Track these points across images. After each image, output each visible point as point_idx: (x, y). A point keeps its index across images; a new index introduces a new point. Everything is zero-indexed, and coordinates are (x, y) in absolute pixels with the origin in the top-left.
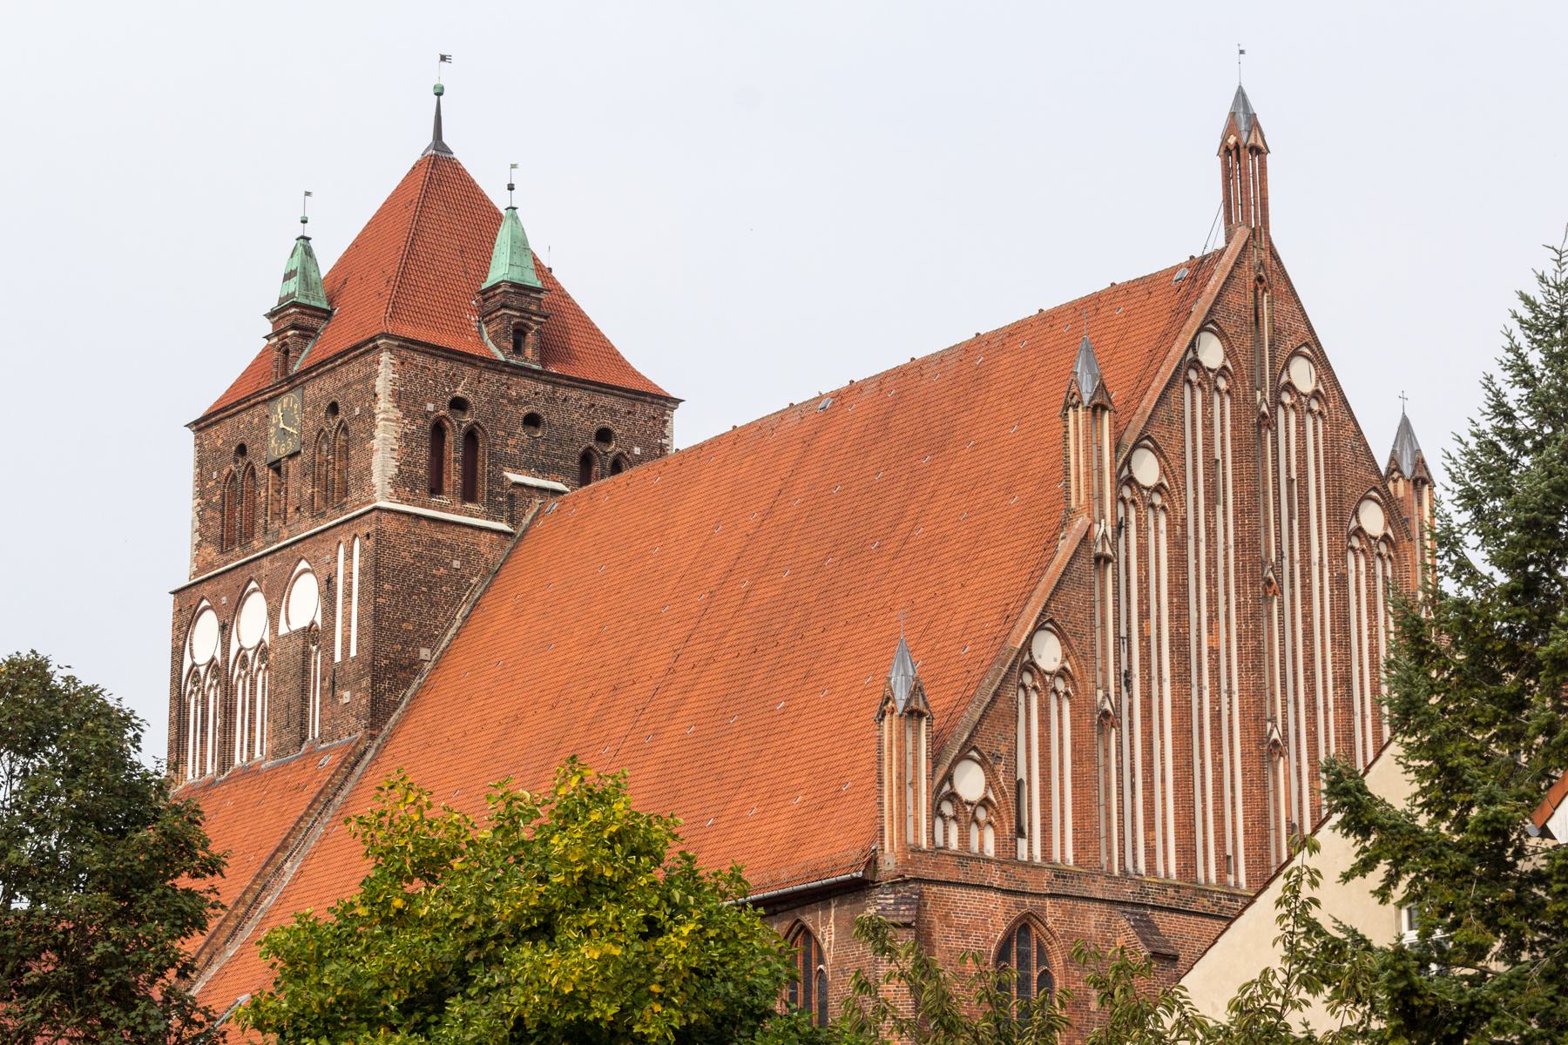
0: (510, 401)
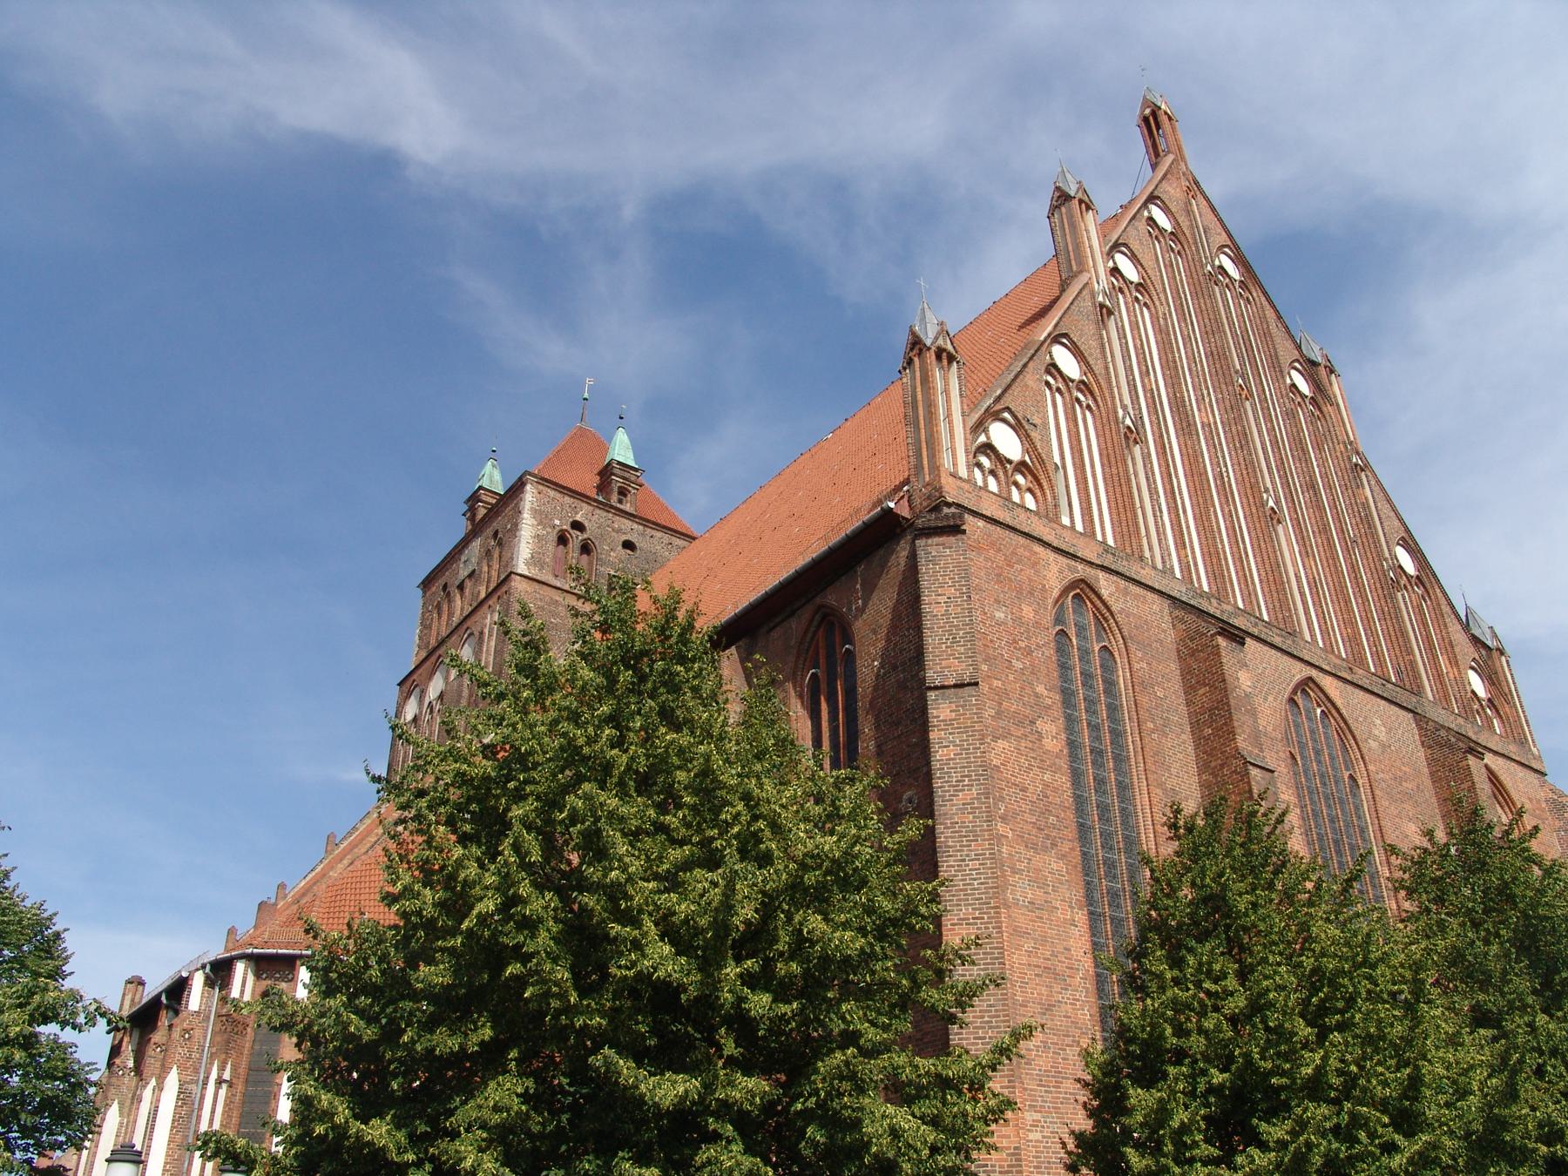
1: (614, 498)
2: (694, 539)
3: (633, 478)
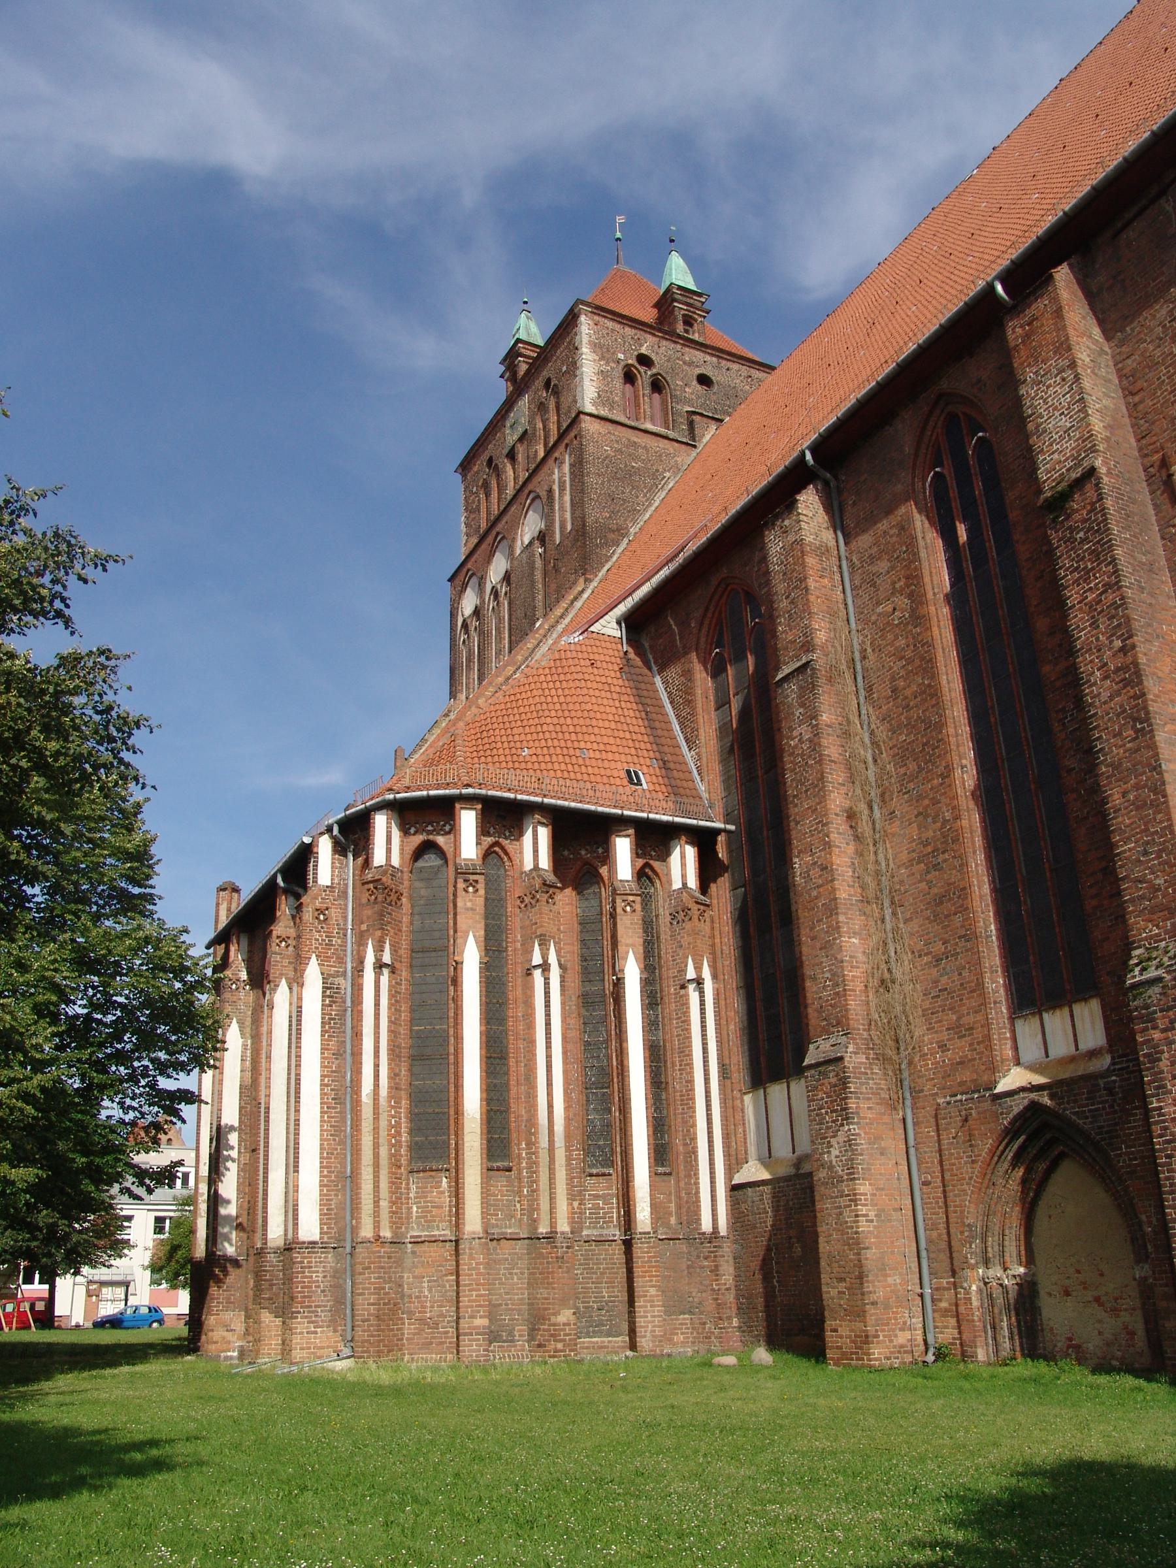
0: (685, 363)
1: (680, 328)
2: (773, 368)
3: (699, 305)
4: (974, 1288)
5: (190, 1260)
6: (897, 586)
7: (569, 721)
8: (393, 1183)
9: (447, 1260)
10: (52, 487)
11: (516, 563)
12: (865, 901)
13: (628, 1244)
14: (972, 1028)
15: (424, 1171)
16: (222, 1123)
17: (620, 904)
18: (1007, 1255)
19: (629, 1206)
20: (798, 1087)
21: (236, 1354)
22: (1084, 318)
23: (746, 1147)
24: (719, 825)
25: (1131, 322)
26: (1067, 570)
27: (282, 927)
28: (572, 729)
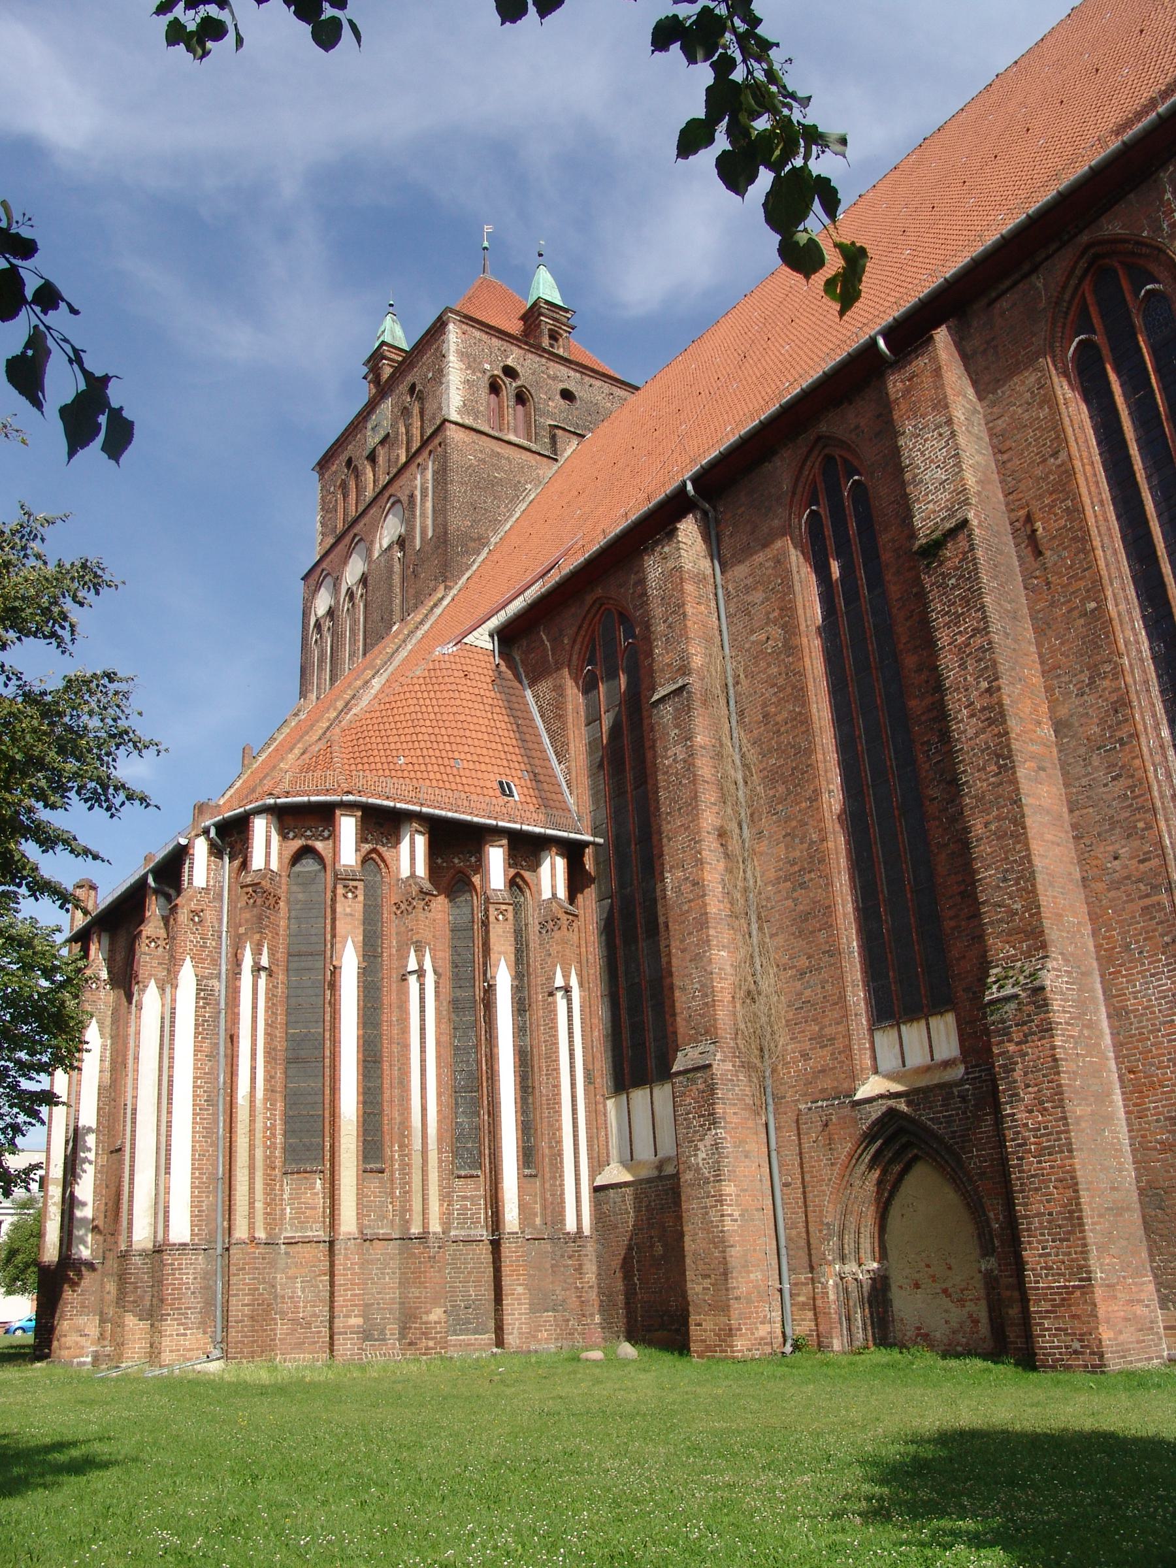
1: (546, 342)
3: (565, 320)
4: (831, 1282)
5: (37, 1263)
6: (771, 616)
7: (443, 731)
8: (267, 1184)
9: (320, 1261)
10: (61, 515)
11: (373, 566)
12: (734, 915)
13: (496, 1245)
14: (834, 1039)
15: (298, 1173)
16: (80, 1125)
17: (492, 912)
18: (862, 1251)
19: (497, 1207)
20: (663, 1093)
21: (89, 1359)
22: (960, 378)
23: (608, 1149)
24: (588, 838)
25: (1003, 386)
26: (939, 613)
27: (152, 927)
28: (446, 739)
